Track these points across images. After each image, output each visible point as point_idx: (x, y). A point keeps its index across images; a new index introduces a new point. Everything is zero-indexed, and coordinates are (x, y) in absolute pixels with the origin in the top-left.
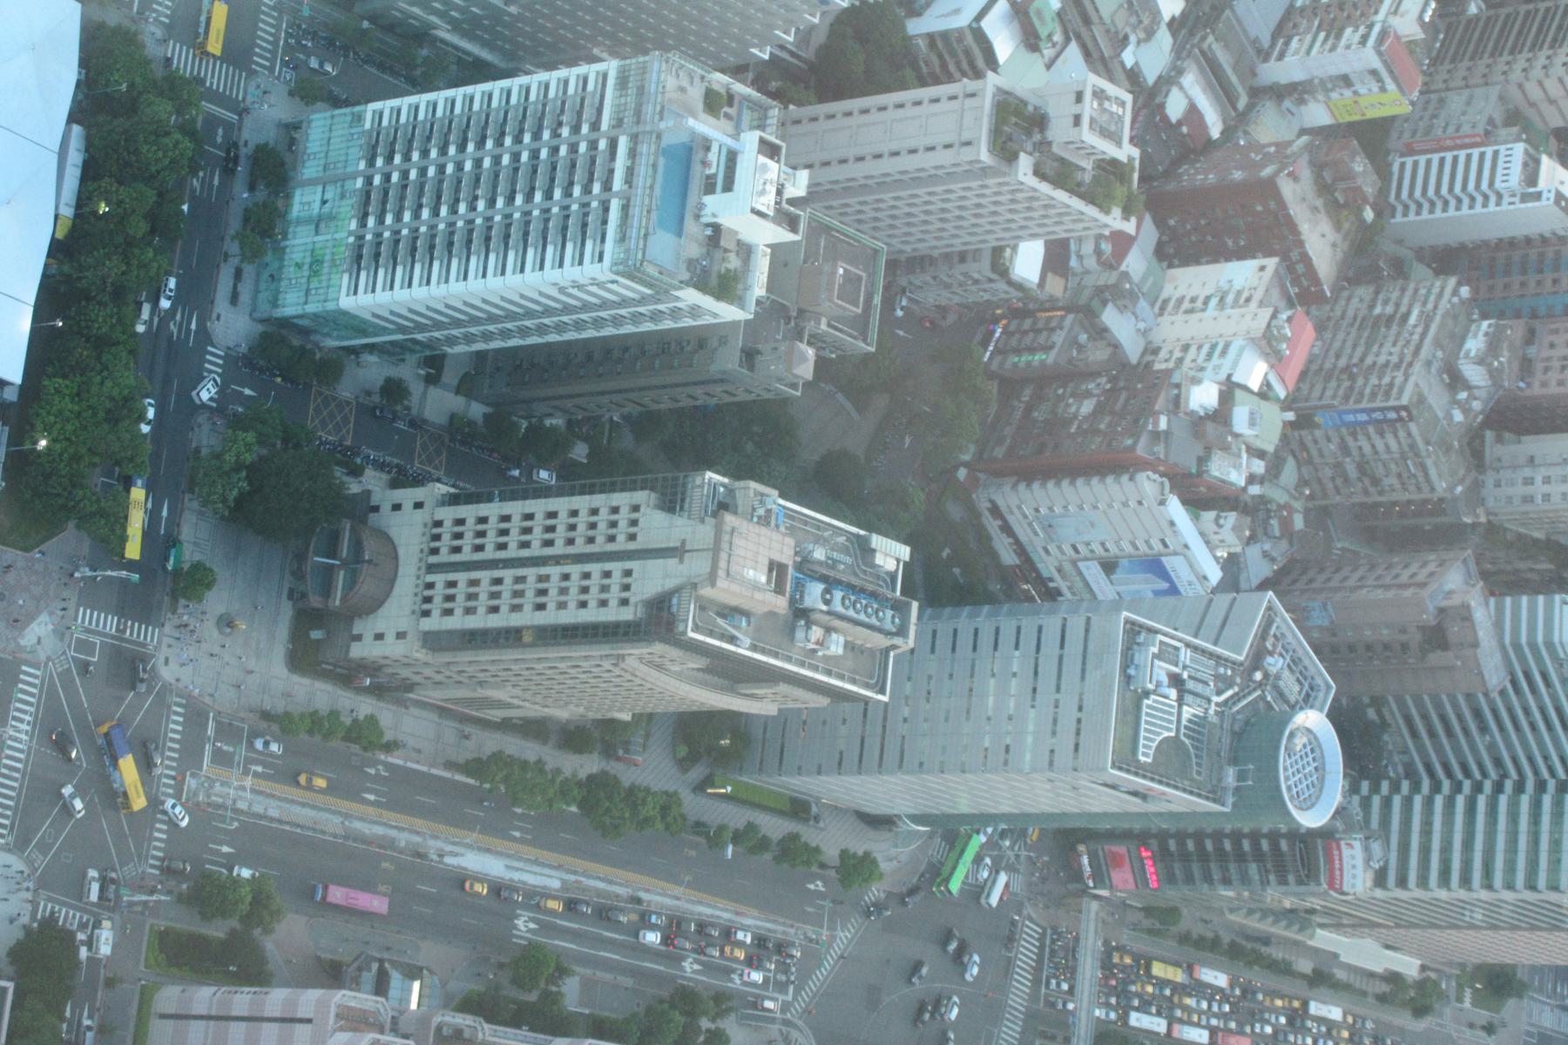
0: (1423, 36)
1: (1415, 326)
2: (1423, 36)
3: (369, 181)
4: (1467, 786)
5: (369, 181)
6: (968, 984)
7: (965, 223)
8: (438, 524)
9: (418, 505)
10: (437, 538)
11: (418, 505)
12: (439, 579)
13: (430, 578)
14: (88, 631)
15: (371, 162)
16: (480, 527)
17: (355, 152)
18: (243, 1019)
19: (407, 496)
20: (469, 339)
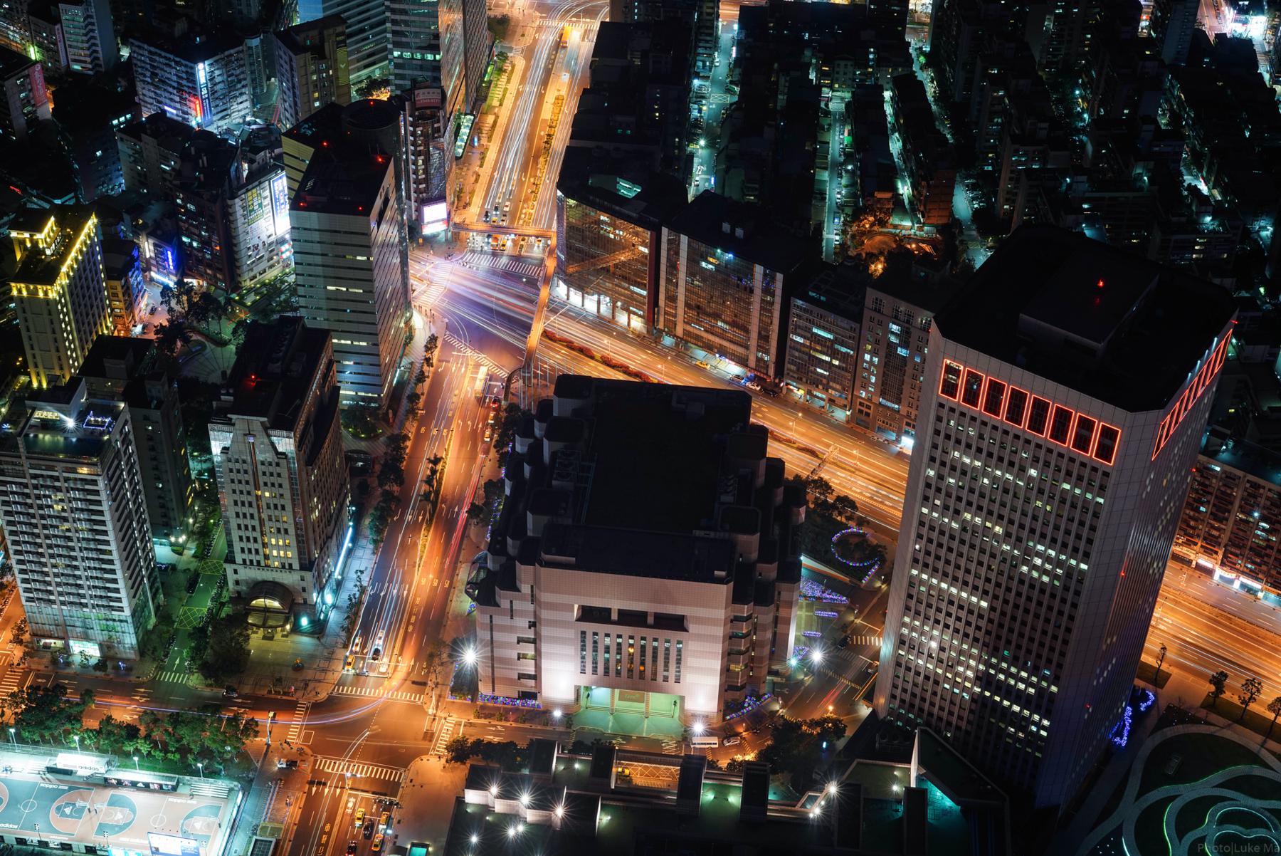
0: (1235, 279)
1: (699, 370)
2: (1235, 279)
3: (63, 603)
4: (388, 14)
5: (63, 603)
6: (910, 572)
7: (90, 276)
8: (244, 561)
9: (236, 572)
10: (251, 561)
11: (236, 572)
12: (262, 480)
13: (261, 484)
14: (299, 737)
15: (53, 602)
16: (246, 551)
17: (49, 610)
18: (492, 638)
19: (231, 578)
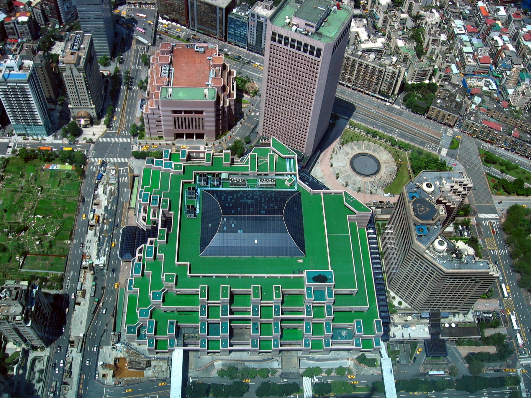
20: (45, 104)
